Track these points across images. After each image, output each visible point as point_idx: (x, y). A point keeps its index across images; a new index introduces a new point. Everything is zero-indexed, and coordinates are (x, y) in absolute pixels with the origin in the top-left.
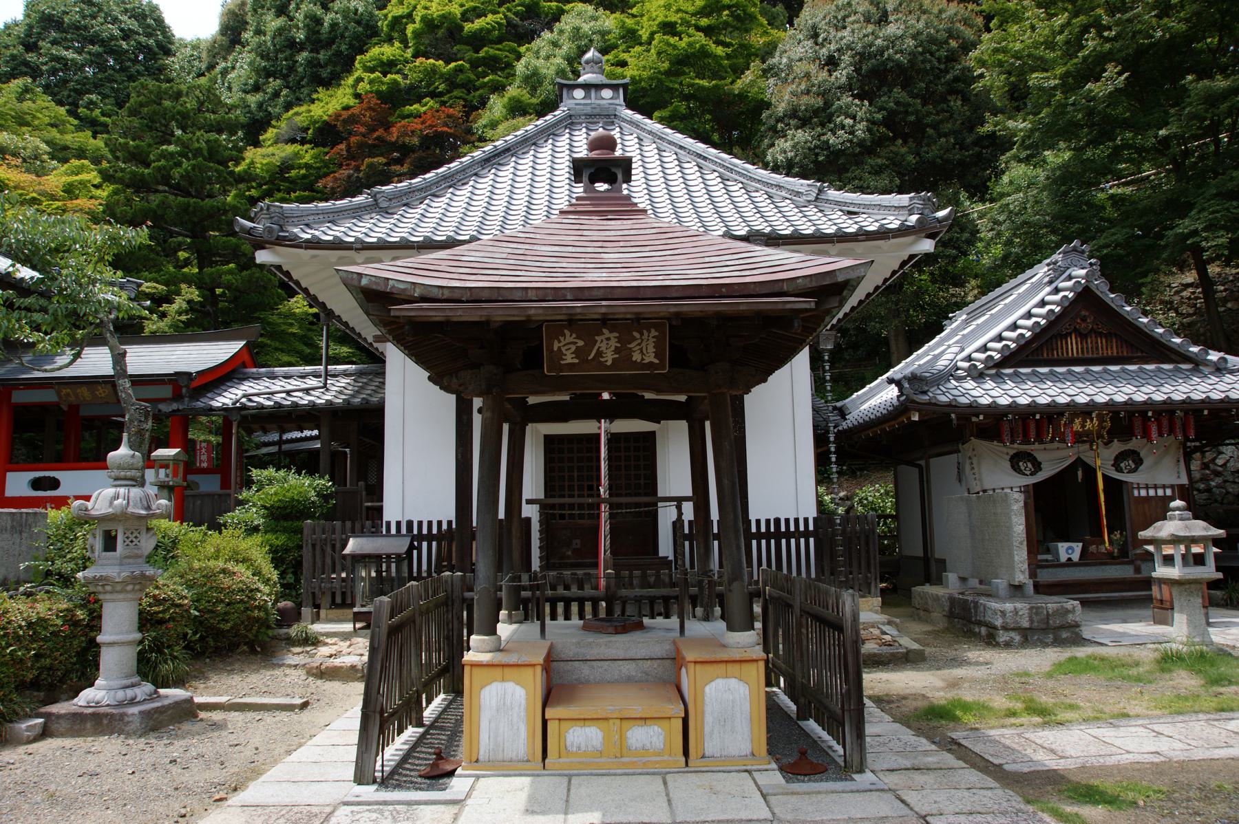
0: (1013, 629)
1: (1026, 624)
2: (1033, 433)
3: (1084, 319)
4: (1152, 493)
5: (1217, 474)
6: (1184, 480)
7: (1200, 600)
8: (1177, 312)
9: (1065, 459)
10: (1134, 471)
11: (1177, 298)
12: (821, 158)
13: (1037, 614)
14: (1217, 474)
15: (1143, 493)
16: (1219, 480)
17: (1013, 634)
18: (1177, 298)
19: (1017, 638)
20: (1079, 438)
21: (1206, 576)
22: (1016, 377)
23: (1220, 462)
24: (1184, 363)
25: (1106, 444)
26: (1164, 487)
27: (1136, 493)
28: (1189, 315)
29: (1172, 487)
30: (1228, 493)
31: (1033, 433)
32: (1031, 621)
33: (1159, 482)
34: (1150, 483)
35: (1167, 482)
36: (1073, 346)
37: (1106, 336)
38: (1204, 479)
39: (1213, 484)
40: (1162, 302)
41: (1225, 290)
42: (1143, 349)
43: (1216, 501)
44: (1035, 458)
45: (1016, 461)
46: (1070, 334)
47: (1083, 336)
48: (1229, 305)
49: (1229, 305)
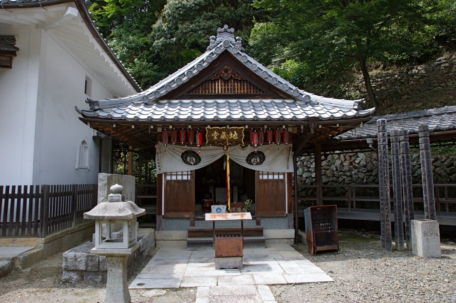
0: (72, 271)
1: (82, 267)
2: (183, 139)
3: (226, 71)
4: (271, 177)
5: (356, 168)
6: (291, 170)
7: (121, 271)
8: (360, 91)
9: (215, 156)
10: (261, 163)
11: (360, 84)
12: (181, 13)
13: (91, 260)
14: (356, 168)
15: (265, 177)
16: (356, 171)
17: (72, 274)
18: (360, 84)
19: (75, 277)
20: (220, 143)
21: (123, 252)
22: (170, 105)
23: (357, 161)
24: (288, 99)
25: (243, 147)
26: (279, 174)
27: (261, 177)
28: (365, 92)
29: (284, 174)
30: (359, 177)
31: (183, 139)
32: (87, 265)
33: (276, 171)
34: (271, 171)
35: (280, 171)
36: (219, 87)
37: (240, 81)
38: (350, 170)
39: (353, 173)
40: (354, 86)
41: (381, 81)
42: (265, 90)
43: (354, 182)
44: (198, 155)
45: (184, 157)
46: (218, 80)
47: (226, 82)
48: (382, 88)
49: (382, 88)
